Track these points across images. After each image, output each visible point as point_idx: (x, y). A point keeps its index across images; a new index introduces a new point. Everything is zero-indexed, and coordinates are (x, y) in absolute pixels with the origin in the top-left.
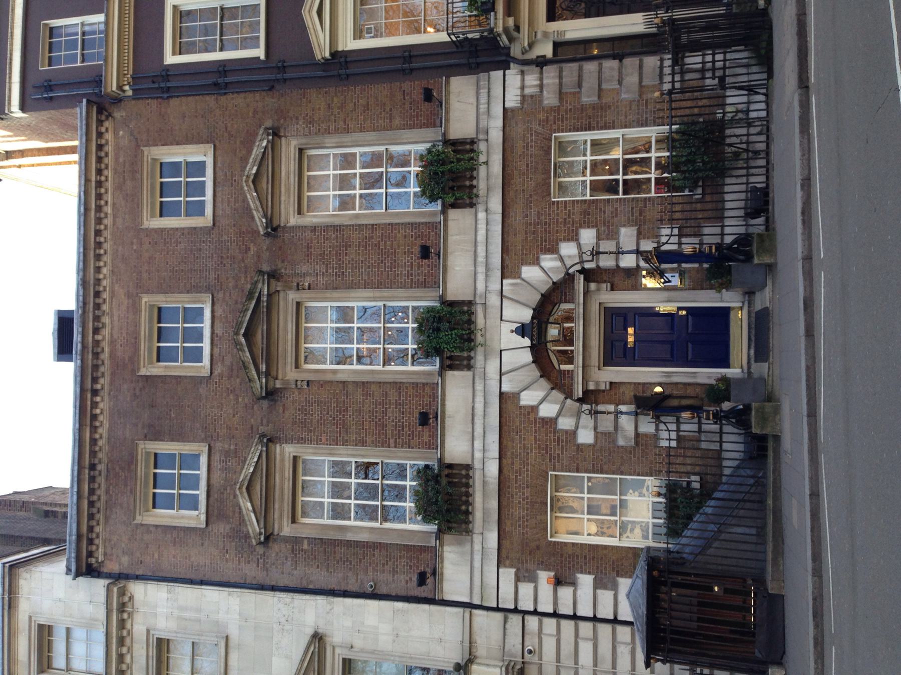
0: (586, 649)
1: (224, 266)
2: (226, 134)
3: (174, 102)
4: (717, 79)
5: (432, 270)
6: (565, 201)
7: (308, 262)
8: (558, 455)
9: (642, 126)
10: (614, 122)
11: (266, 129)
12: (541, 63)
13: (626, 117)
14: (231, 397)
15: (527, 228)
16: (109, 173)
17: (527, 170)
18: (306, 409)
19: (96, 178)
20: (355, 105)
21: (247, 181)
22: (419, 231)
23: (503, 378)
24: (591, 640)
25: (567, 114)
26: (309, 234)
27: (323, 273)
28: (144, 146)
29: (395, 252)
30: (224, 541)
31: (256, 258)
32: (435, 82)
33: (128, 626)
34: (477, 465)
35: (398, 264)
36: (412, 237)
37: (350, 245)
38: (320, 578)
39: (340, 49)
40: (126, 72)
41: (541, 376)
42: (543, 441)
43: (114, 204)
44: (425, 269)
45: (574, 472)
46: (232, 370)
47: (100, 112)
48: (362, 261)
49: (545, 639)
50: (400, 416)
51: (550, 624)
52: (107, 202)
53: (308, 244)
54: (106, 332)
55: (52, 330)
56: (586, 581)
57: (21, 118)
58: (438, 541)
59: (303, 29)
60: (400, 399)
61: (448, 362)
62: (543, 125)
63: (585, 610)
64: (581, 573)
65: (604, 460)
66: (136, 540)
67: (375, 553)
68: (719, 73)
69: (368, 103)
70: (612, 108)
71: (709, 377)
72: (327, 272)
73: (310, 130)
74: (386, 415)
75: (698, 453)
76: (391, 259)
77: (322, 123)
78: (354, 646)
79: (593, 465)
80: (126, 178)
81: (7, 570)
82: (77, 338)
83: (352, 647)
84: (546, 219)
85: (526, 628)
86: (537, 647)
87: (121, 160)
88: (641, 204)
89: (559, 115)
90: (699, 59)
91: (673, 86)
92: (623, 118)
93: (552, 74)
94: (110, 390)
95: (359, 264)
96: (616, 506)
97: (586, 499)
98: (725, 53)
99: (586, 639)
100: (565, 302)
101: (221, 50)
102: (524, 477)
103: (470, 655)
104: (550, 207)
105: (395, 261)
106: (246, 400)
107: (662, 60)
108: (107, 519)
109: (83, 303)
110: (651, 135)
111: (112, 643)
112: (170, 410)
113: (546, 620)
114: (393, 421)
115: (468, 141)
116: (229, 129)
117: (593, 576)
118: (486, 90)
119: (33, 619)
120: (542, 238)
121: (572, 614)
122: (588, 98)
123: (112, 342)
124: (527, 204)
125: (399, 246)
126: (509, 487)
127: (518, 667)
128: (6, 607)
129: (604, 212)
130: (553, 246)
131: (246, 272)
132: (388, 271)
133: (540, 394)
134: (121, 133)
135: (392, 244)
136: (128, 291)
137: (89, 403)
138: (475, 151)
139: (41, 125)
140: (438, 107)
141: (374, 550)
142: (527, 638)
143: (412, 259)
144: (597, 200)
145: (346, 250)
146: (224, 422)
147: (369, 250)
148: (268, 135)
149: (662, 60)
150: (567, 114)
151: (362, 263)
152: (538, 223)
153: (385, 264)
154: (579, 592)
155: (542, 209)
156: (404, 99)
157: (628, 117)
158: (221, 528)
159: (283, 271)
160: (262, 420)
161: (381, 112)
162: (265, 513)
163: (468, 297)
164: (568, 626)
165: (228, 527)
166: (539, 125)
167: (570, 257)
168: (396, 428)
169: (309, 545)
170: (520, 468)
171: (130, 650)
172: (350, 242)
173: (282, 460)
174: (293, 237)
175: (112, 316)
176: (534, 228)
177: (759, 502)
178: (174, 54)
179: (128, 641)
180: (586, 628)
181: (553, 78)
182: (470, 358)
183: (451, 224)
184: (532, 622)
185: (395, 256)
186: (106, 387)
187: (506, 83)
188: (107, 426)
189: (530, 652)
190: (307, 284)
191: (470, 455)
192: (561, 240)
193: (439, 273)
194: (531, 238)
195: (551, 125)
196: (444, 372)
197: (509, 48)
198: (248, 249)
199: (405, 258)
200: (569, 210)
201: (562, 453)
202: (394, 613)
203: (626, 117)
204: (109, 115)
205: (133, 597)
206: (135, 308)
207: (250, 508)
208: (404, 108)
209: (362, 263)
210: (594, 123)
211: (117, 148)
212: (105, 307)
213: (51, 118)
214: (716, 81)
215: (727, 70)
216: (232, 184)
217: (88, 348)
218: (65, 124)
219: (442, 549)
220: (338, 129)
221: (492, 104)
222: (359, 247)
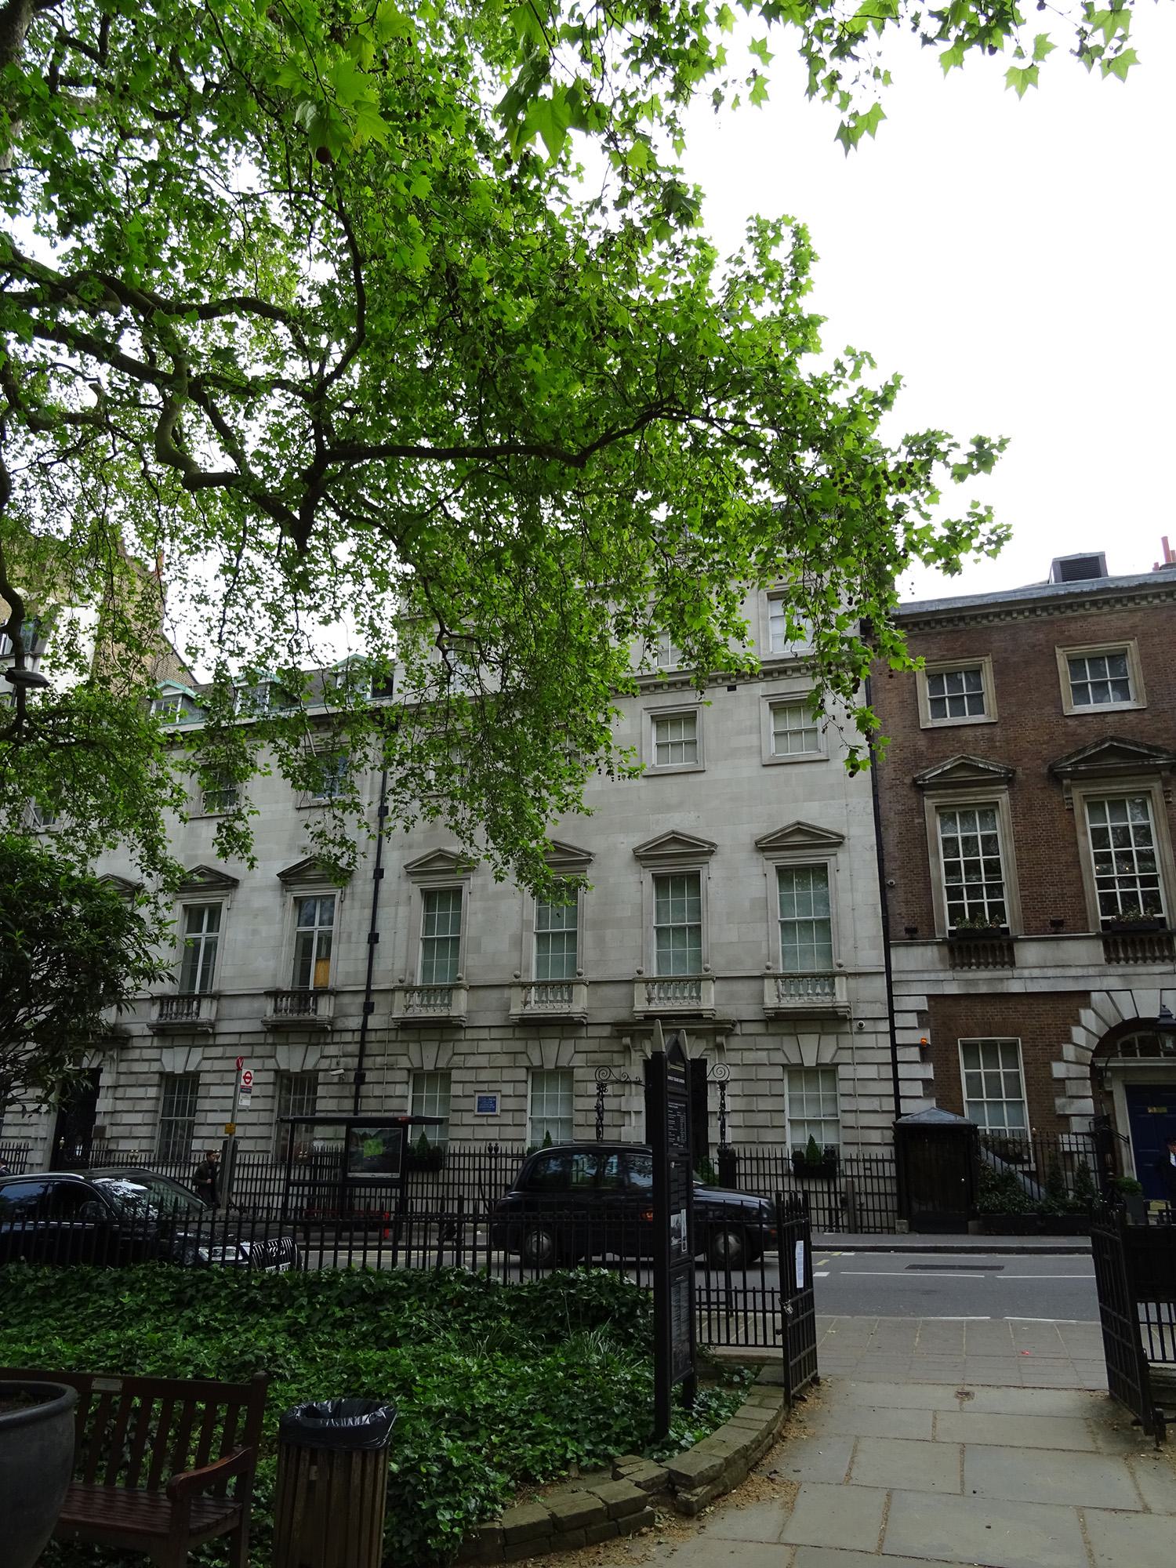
38: (891, 837)
54: (1094, 610)
158: (922, 743)
162: (943, 783)
173: (992, 792)
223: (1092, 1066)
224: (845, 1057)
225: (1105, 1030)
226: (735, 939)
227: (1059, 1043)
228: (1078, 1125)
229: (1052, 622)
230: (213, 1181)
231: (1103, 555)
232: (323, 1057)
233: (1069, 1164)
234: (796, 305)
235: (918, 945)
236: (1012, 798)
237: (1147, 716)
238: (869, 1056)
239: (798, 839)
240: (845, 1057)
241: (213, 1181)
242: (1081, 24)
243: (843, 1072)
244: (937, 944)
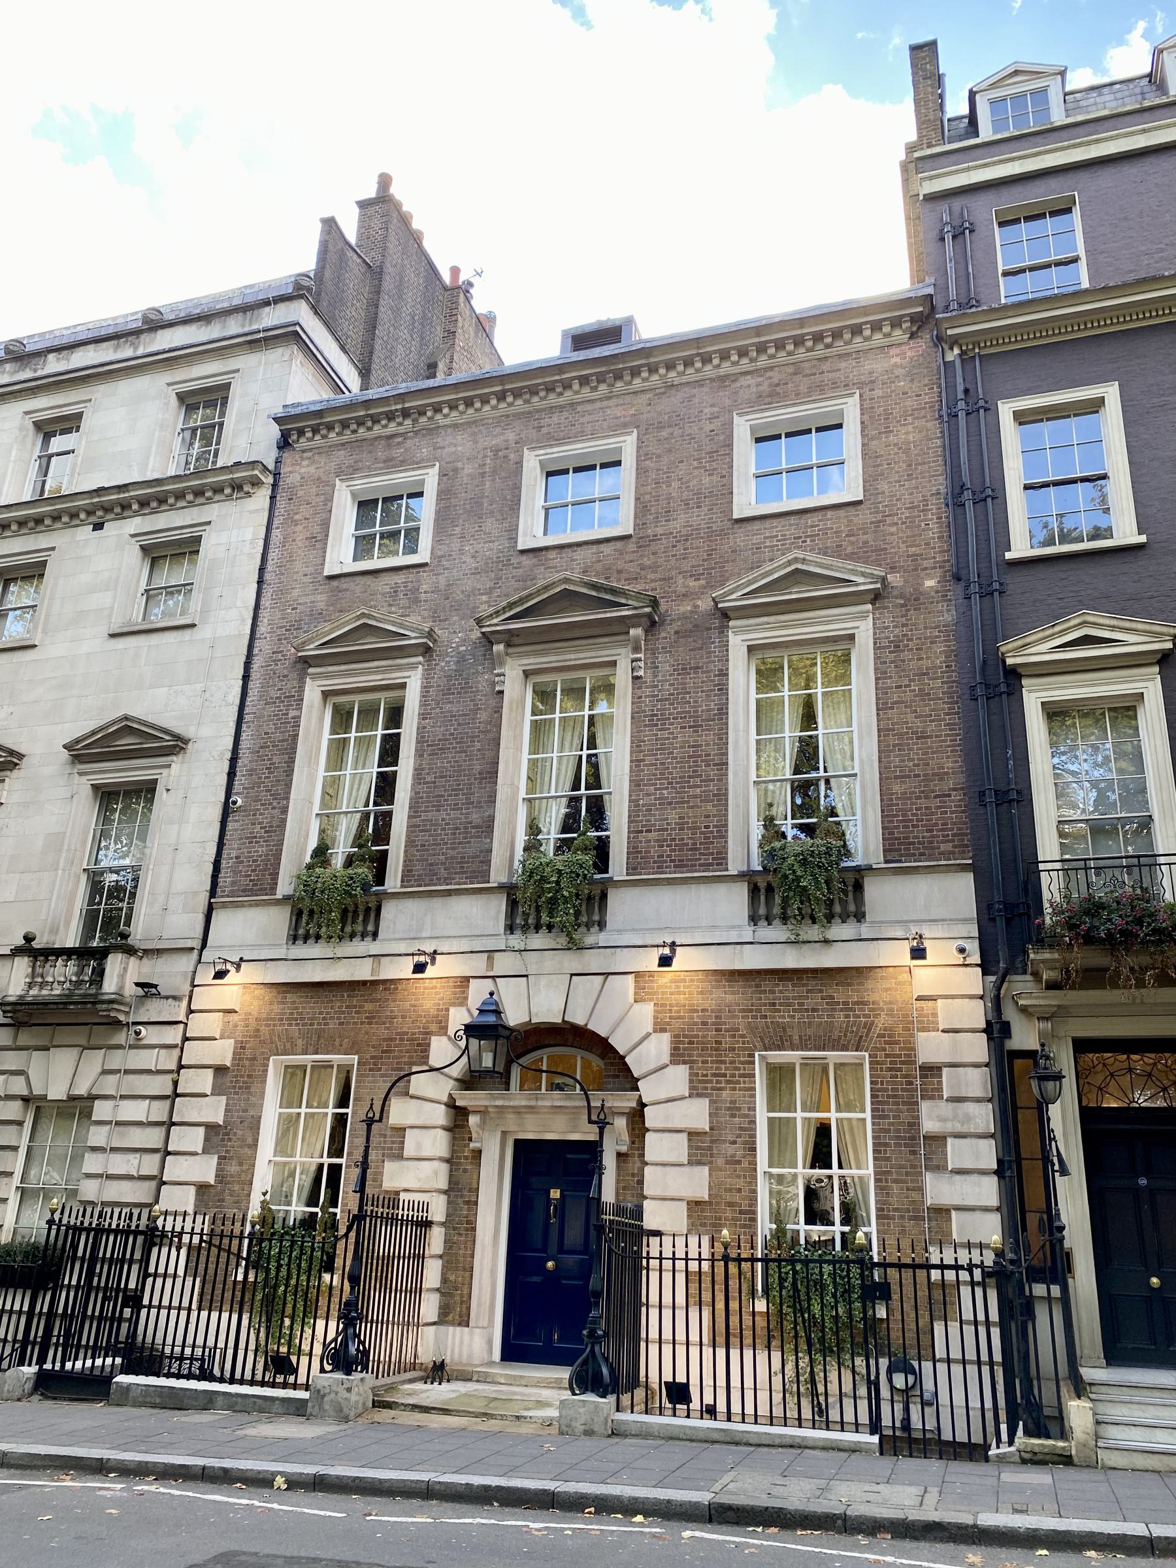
2: (880, 516)
3: (934, 428)
6: (754, 1076)
8: (380, 1069)
10: (887, 1159)
11: (883, 580)
12: (997, 1030)
17: (807, 1010)
19: (808, 334)
21: (796, 560)
22: (714, 837)
23: (490, 980)
25: (903, 1076)
26: (715, 667)
28: (861, 396)
31: (684, 590)
32: (967, 846)
33: (217, 498)
36: (705, 827)
39: (1024, 682)
40: (982, 345)
44: (656, 852)
47: (913, 319)
54: (586, 393)
55: (612, 317)
56: (932, 1117)
59: (1054, 617)
61: (762, 885)
69: (930, 737)
70: (912, 1157)
73: (884, 647)
75: (924, 1321)
77: (896, 667)
81: (291, 329)
83: (168, 790)
86: (144, 1042)
89: (902, 1063)
91: (935, 1267)
97: (298, 1110)
103: (144, 950)
104: (744, 1049)
105: (671, 803)
109: (646, 351)
111: (17, 511)
119: (88, 404)
120: (697, 1036)
122: (932, 1117)
124: (751, 1011)
125: (692, 807)
127: (122, 1018)
128: (249, 338)
130: (683, 1055)
131: (664, 579)
137: (486, 391)
138: (829, 922)
145: (690, 727)
147: (688, 762)
150: (903, 1076)
153: (667, 788)
161: (913, 760)
171: (191, 504)
173: (400, 668)
174: (714, 642)
177: (799, 1419)
179: (201, 500)
182: (769, 920)
183: (722, 889)
185: (677, 803)
189: (138, 1033)
190: (641, 673)
192: (690, 1068)
196: (504, 890)
197: (1025, 973)
206: (621, 427)
208: (919, 798)
217: (322, 418)
220: (886, 693)
222: (694, 746)
223: (451, 1105)
224: (109, 1085)
232: (105, 1072)
236: (427, 677)
237: (631, 546)
239: (127, 742)
240: (109, 1085)
243: (101, 1110)
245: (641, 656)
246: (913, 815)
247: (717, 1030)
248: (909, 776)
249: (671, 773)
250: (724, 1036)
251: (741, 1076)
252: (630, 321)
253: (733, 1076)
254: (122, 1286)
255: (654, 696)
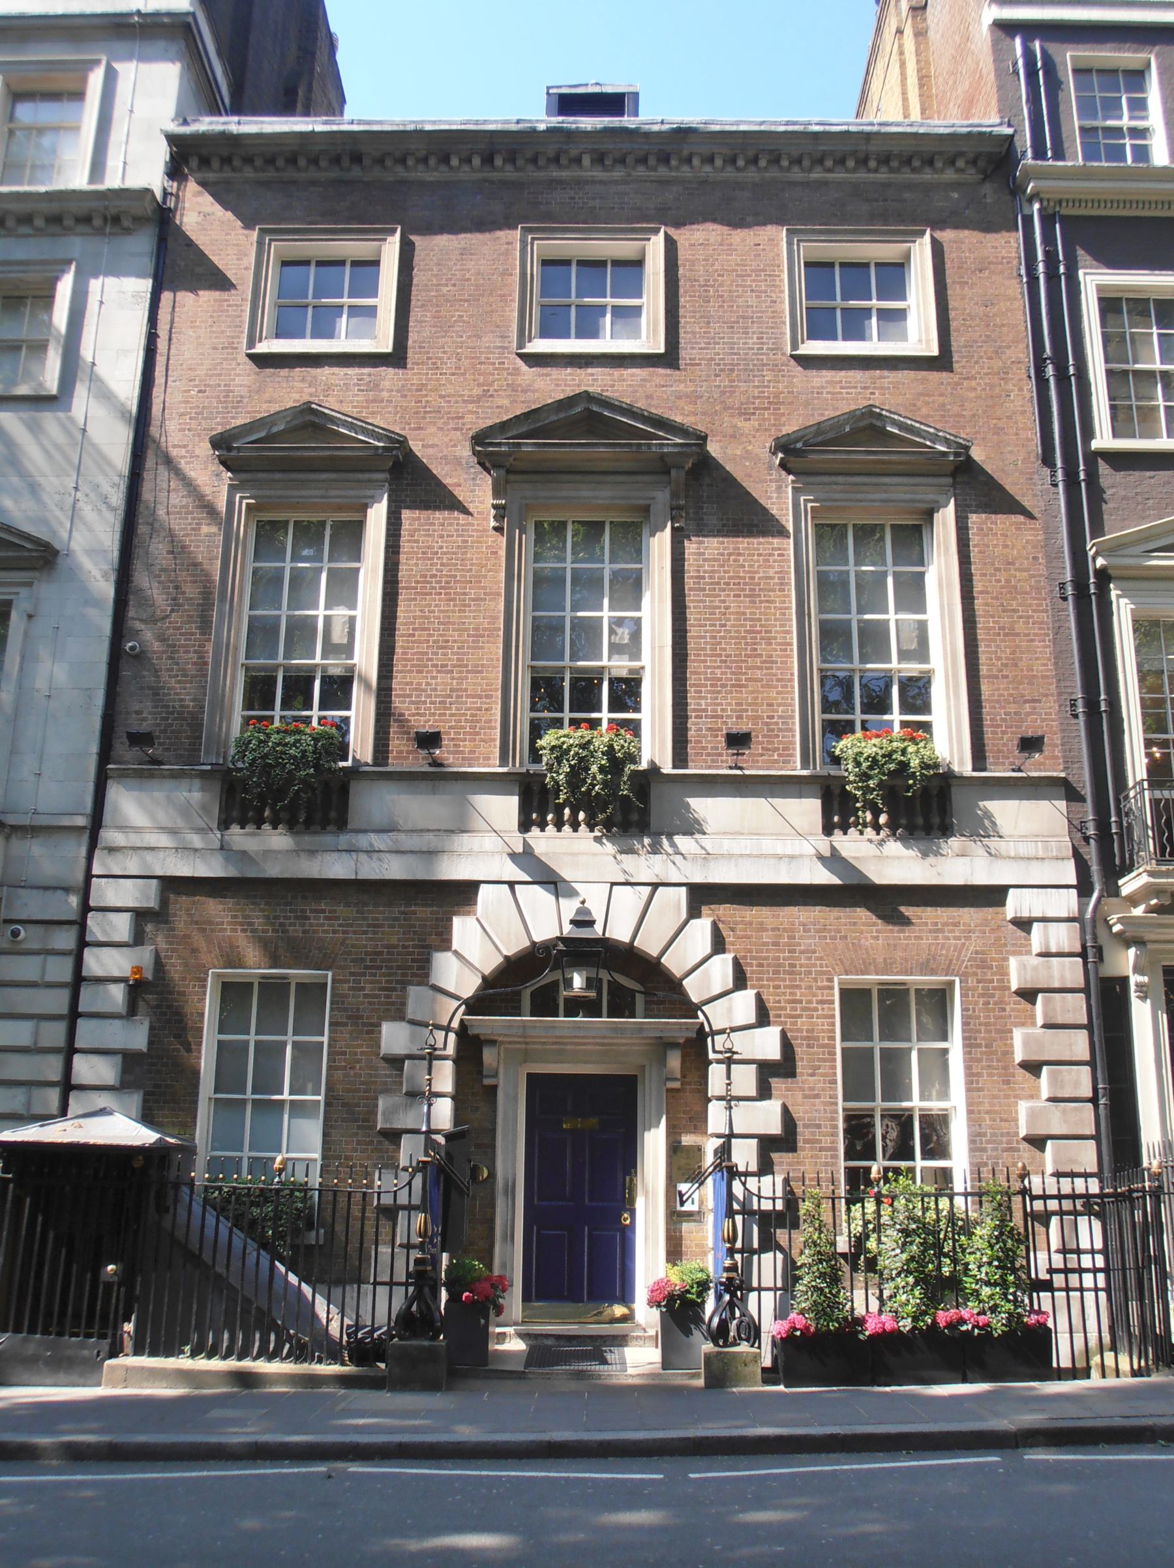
0: (19, 1033)
1: (716, 376)
4: (1048, 1277)
5: (708, 755)
7: (724, 526)
9: (972, 1142)
13: (988, 1112)
14: (477, 391)
15: (785, 930)
16: (882, 176)
18: (451, 524)
20: (1013, 610)
24: (36, 1043)
27: (704, 554)
29: (740, 686)
30: (219, 385)
33: (81, 228)
34: (344, 839)
35: (719, 692)
36: (768, 717)
37: (754, 602)
41: (484, 978)
42: (390, 960)
43: (826, 183)
45: (330, 1017)
46: (525, 391)
48: (725, 625)
49: (37, 960)
50: (436, 696)
51: (62, 970)
52: (829, 170)
53: (757, 526)
57: (980, 23)
58: (209, 767)
60: (468, 696)
62: (975, 959)
63: (87, 1032)
64: (152, 1028)
65: (352, 1073)
66: (227, 234)
67: (191, 655)
68: (1059, 1280)
69: (1018, 635)
71: (503, 1266)
72: (705, 560)
74: (438, 672)
76: (727, 679)
78: (25, 618)
79: (345, 1053)
80: (875, 204)
82: (588, 123)
84: (801, 966)
85: (56, 928)
87: (907, 195)
88: (826, 1141)
90: (1085, 1244)
92: (987, 1107)
93: (1068, 975)
94: (492, 182)
95: (720, 619)
96: (686, 767)
98: (1096, 1289)
99: (36, 1034)
100: (646, 1002)
101: (1110, 373)
102: (322, 925)
104: (822, 973)
106: (469, 418)
107: (1086, 1175)
108: (266, 184)
110: (315, 517)
112: (454, 285)
113: (68, 964)
114: (428, 684)
115: (947, 821)
116: (966, 383)
117: (145, 1050)
118: (1041, 854)
120: (766, 958)
121: (80, 1010)
123: (579, 183)
126: (305, 898)
129: (812, 1075)
132: (706, 673)
133: (474, 956)
134: (956, 195)
135: (756, 680)
136: (670, 208)
139: (969, 60)
140: (1012, 764)
141: (195, 652)
142: (39, 929)
143: (728, 717)
144: (834, 1060)
146: (430, 380)
148: (957, 454)
149: (1086, 1175)
151: (722, 626)
152: (794, 951)
154: (117, 1023)
155: (821, 959)
156: (1026, 702)
157: (987, 1116)
159: (707, 480)
160: (432, 446)
163: (353, 822)
164: (58, 1002)
165: (244, 392)
166: (977, 953)
167: (730, 1010)
168: (416, 689)
169: (208, 535)
170: (337, 918)
172: (761, 602)
175: (624, 182)
176: (785, 944)
178: (1100, 288)
179: (56, 229)
180: (55, 1034)
181: (1062, 977)
184: (65, 939)
186: (495, 175)
187: (1053, 890)
188: (429, 179)
189: (15, 934)
191: (363, 827)
193: (701, 768)
194: (767, 937)
195: (976, 974)
198: (746, 415)
199: (730, 704)
200: (816, 1009)
201: (366, 996)
202: (87, 689)
203: (988, 1112)
204: (986, 177)
205: (130, 234)
207: (275, 430)
209: (722, 626)
210: (977, 1053)
211: (928, 188)
212: (641, 171)
213: (981, 76)
214: (1043, 1276)
215: (1064, 1294)
216: (867, 388)
218: (971, 102)
219: (196, 776)
221: (1014, 865)
222: (751, 620)
225: (495, 962)
226: (882, 1221)
227: (404, 984)
228: (410, 1151)
229: (518, 186)
230: (331, 1234)
231: (636, 95)
233: (385, 1230)
234: (945, 1327)
235: (163, 776)
238: (22, 1000)
241: (331, 1234)
242: (859, 734)
244: (203, 775)
245: (682, 502)
246: (1002, 720)
247: (794, 951)
248: (996, 677)
249: (725, 649)
250: (799, 959)
251: (819, 1002)
252: (636, 95)
253: (809, 1002)
254: (1029, 1209)
255: (700, 554)
